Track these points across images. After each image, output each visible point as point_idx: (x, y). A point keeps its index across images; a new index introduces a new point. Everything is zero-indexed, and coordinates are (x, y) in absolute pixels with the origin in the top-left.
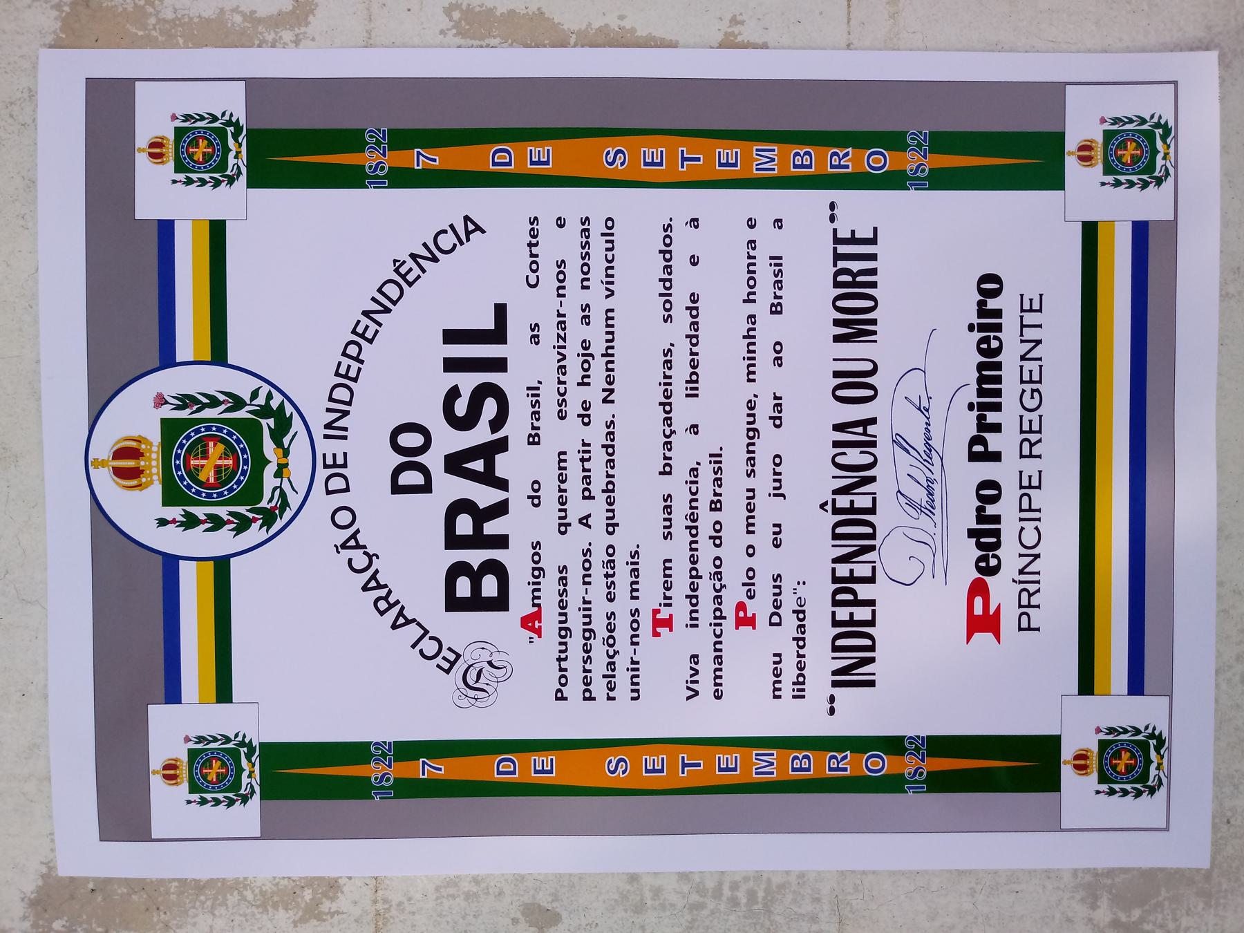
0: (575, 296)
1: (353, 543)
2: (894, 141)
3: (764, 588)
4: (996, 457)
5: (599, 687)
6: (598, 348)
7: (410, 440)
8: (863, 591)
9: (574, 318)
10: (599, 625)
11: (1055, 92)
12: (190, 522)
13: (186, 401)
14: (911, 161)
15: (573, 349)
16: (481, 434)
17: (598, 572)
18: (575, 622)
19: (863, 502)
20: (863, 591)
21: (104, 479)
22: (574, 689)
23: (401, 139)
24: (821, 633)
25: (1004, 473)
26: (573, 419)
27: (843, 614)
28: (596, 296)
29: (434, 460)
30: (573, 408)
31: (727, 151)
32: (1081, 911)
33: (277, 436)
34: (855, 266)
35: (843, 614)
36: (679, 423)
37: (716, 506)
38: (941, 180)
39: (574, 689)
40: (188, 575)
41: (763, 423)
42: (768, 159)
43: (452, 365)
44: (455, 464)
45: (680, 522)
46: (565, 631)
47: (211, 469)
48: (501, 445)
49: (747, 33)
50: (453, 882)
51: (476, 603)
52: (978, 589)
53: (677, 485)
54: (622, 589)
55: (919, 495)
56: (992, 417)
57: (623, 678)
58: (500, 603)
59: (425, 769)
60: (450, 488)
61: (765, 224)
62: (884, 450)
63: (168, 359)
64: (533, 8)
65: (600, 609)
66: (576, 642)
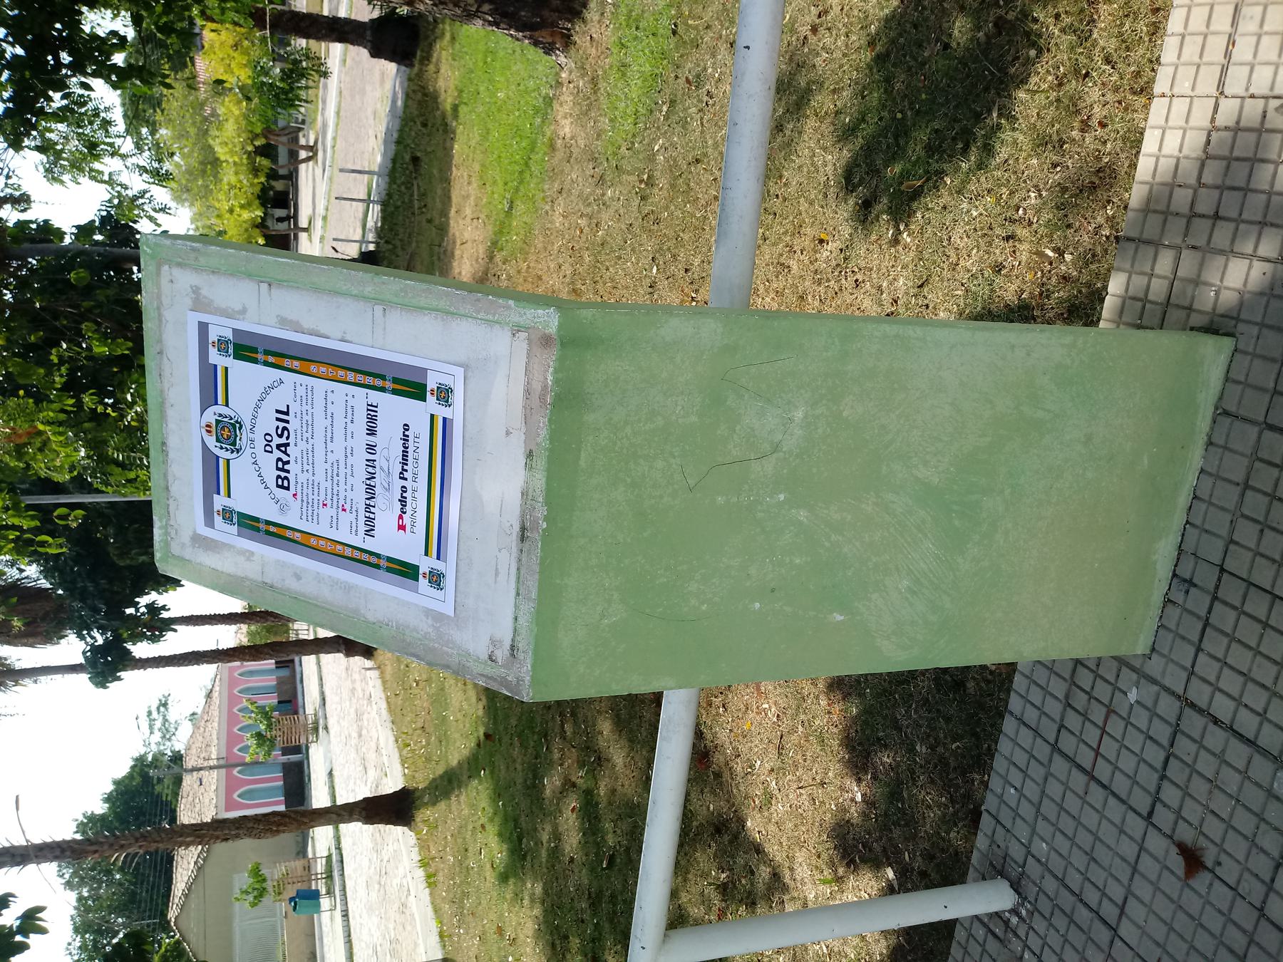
0: (305, 407)
1: (255, 463)
2: (383, 378)
3: (348, 501)
4: (406, 479)
5: (310, 518)
6: (310, 423)
7: (268, 438)
8: (372, 510)
9: (304, 413)
10: (310, 501)
11: (424, 371)
12: (222, 448)
13: (220, 415)
14: (388, 385)
15: (304, 422)
16: (283, 440)
17: (310, 486)
18: (305, 499)
19: (373, 484)
20: (372, 510)
21: (204, 431)
22: (304, 517)
23: (267, 352)
24: (362, 519)
25: (408, 484)
26: (304, 442)
27: (367, 514)
28: (309, 407)
29: (274, 444)
30: (305, 439)
31: (341, 373)
32: (424, 619)
33: (240, 428)
34: (373, 413)
35: (367, 514)
36: (329, 450)
37: (338, 475)
38: (395, 392)
39: (304, 517)
40: (222, 462)
41: (349, 455)
42: (351, 376)
43: (278, 419)
44: (278, 447)
45: (329, 478)
46: (302, 501)
47: (332, 630)
48: (288, 445)
49: (348, 338)
50: (279, 561)
51: (282, 487)
52: (401, 517)
53: (328, 466)
54: (316, 493)
55: (387, 486)
56: (405, 467)
57: (315, 518)
58: (288, 488)
59: (272, 529)
60: (278, 454)
61: (350, 396)
62: (378, 469)
63: (216, 404)
64: (81, 818)
65: (311, 497)
66: (305, 504)
